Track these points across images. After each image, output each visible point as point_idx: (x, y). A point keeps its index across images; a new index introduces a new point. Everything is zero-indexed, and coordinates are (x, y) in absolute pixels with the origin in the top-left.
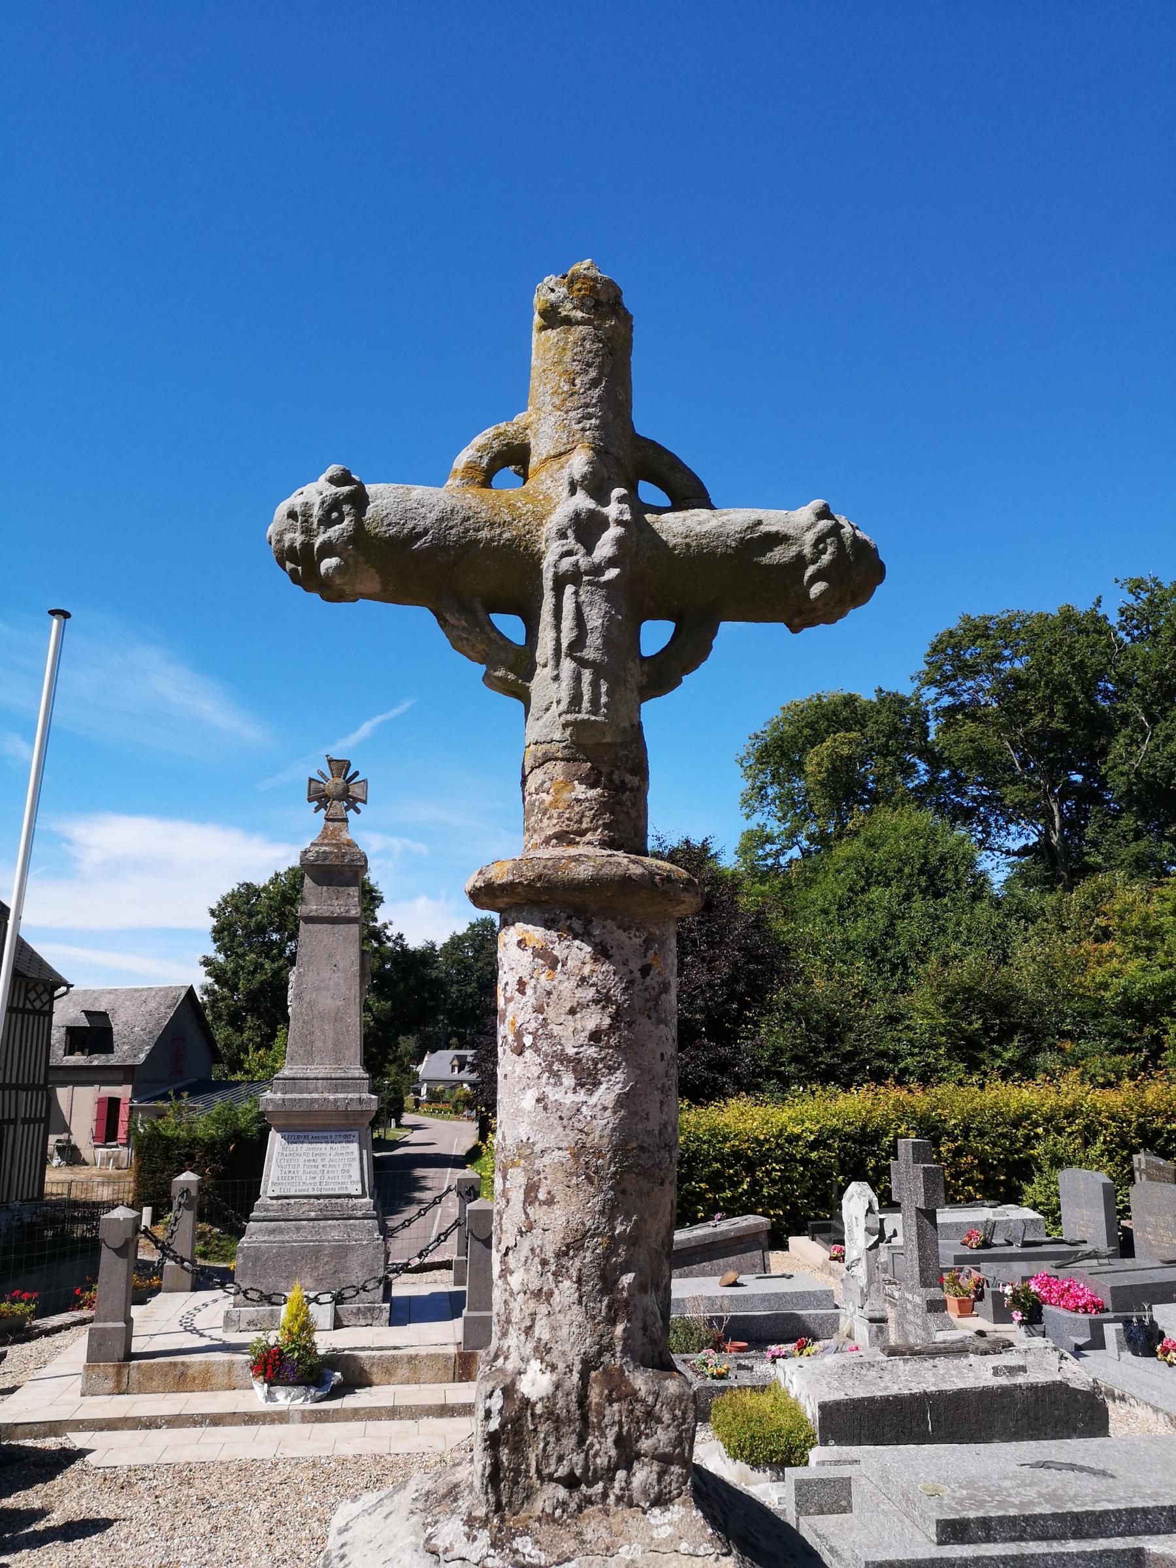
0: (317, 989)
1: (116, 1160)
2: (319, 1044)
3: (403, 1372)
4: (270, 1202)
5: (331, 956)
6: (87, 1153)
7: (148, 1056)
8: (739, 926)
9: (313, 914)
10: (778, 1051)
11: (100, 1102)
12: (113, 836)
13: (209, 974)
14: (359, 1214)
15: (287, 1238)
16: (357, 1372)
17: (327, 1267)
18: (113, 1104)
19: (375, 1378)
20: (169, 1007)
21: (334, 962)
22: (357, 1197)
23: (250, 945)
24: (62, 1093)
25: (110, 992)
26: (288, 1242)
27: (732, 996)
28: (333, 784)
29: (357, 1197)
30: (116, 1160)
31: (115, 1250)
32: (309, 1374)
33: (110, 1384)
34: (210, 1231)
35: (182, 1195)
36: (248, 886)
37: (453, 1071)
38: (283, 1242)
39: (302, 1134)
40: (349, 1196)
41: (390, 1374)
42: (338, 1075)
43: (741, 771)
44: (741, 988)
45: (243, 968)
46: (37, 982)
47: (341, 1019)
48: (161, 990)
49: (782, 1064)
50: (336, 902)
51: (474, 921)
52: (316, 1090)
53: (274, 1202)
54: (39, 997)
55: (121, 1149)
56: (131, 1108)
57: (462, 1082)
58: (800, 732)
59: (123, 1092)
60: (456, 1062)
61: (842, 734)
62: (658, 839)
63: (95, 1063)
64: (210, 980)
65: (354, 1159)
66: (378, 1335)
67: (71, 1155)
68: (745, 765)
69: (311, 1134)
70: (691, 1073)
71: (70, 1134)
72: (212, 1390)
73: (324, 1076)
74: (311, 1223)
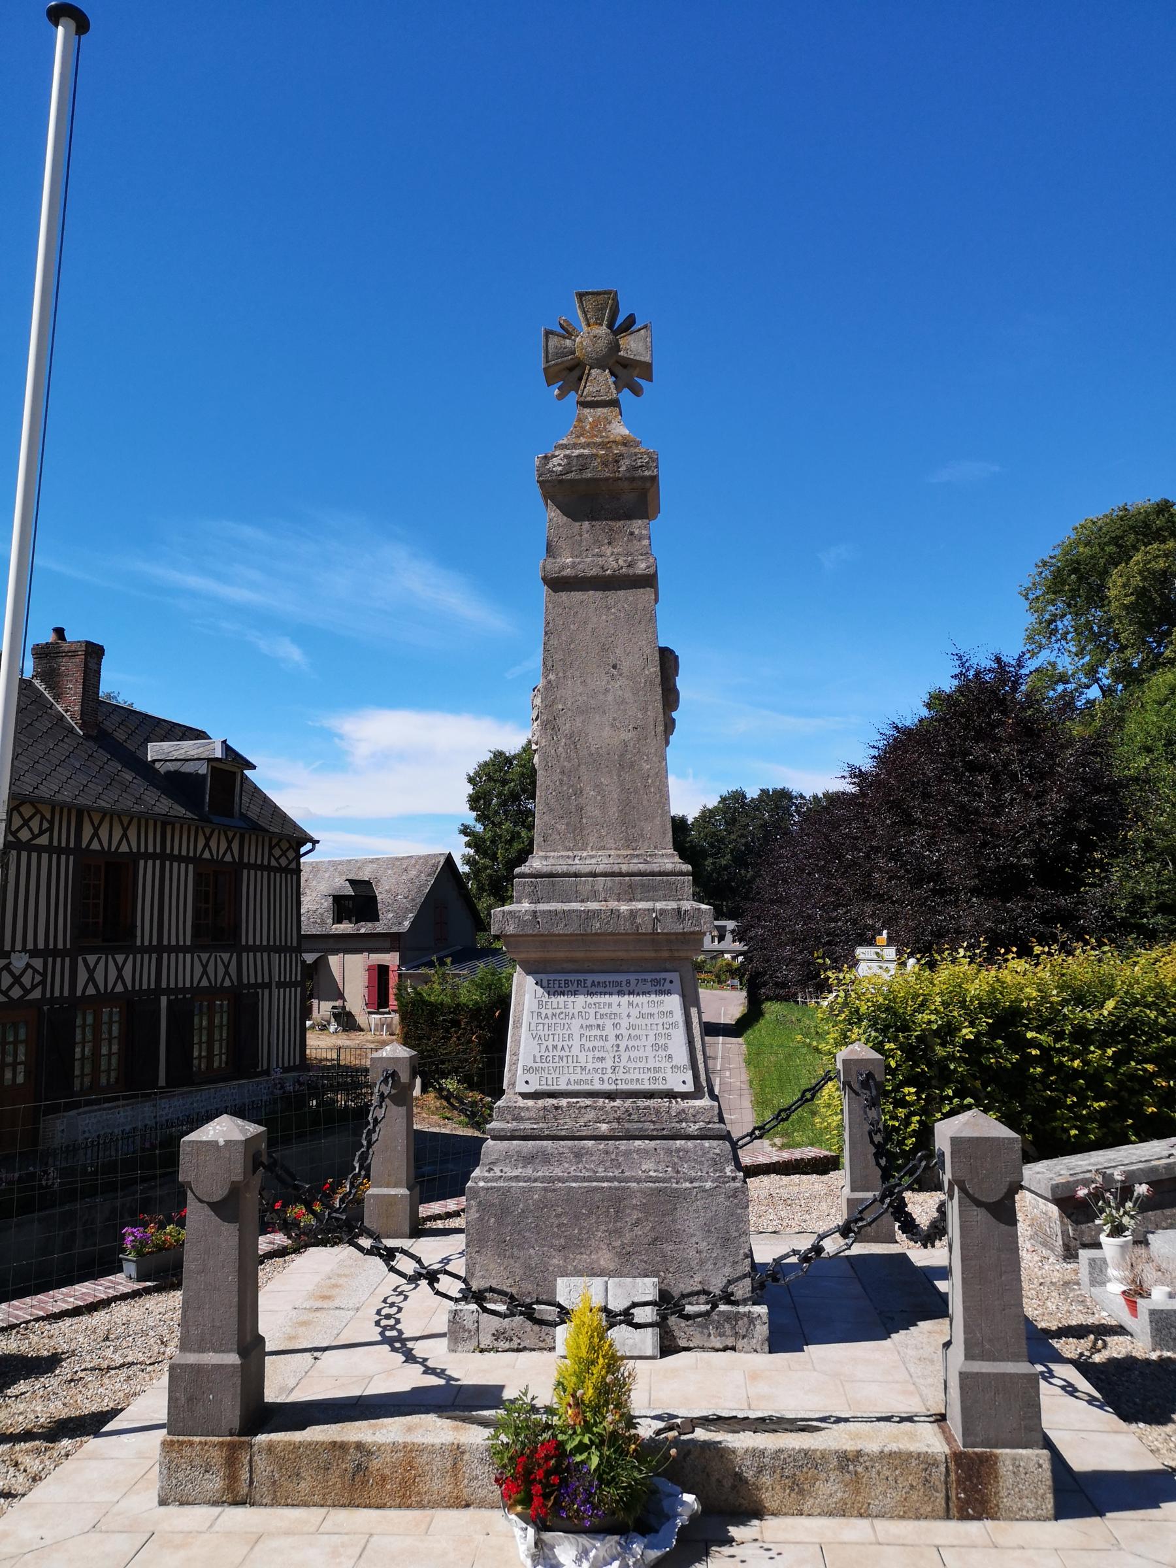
0: (583, 711)
1: (389, 1026)
2: (593, 811)
3: (830, 1488)
4: (521, 1102)
5: (604, 649)
6: (361, 1019)
7: (413, 924)
8: (1069, 757)
9: (567, 572)
10: (1140, 899)
11: (370, 969)
12: (379, 729)
13: (468, 845)
14: (693, 1128)
15: (558, 1172)
16: (727, 1483)
17: (638, 1231)
18: (383, 970)
19: (769, 1499)
20: (429, 875)
21: (612, 660)
22: (685, 1096)
23: (505, 812)
24: (334, 961)
25: (372, 861)
26: (560, 1179)
27: (1069, 835)
28: (589, 337)
29: (685, 1096)
30: (389, 1026)
31: (212, 1206)
32: (628, 1507)
33: (215, 1483)
34: (481, 1100)
35: (385, 1081)
36: (499, 754)
37: (713, 941)
38: (551, 1180)
39: (572, 977)
40: (671, 1095)
41: (801, 1492)
42: (633, 868)
43: (1026, 605)
44: (1082, 825)
45: (500, 837)
46: (281, 837)
47: (632, 765)
48: (420, 857)
49: (1145, 915)
50: (608, 550)
51: (725, 793)
52: (594, 896)
53: (530, 1103)
54: (284, 853)
55: (393, 1015)
56: (400, 975)
57: (723, 952)
58: (1103, 550)
59: (391, 959)
60: (715, 933)
61: (1155, 546)
62: (960, 658)
63: (363, 931)
64: (471, 852)
65: (674, 1025)
66: (754, 1376)
67: (346, 1021)
68: (1031, 597)
69: (590, 978)
70: (1022, 928)
71: (345, 1000)
72: (421, 1506)
73: (608, 869)
74: (602, 1145)
